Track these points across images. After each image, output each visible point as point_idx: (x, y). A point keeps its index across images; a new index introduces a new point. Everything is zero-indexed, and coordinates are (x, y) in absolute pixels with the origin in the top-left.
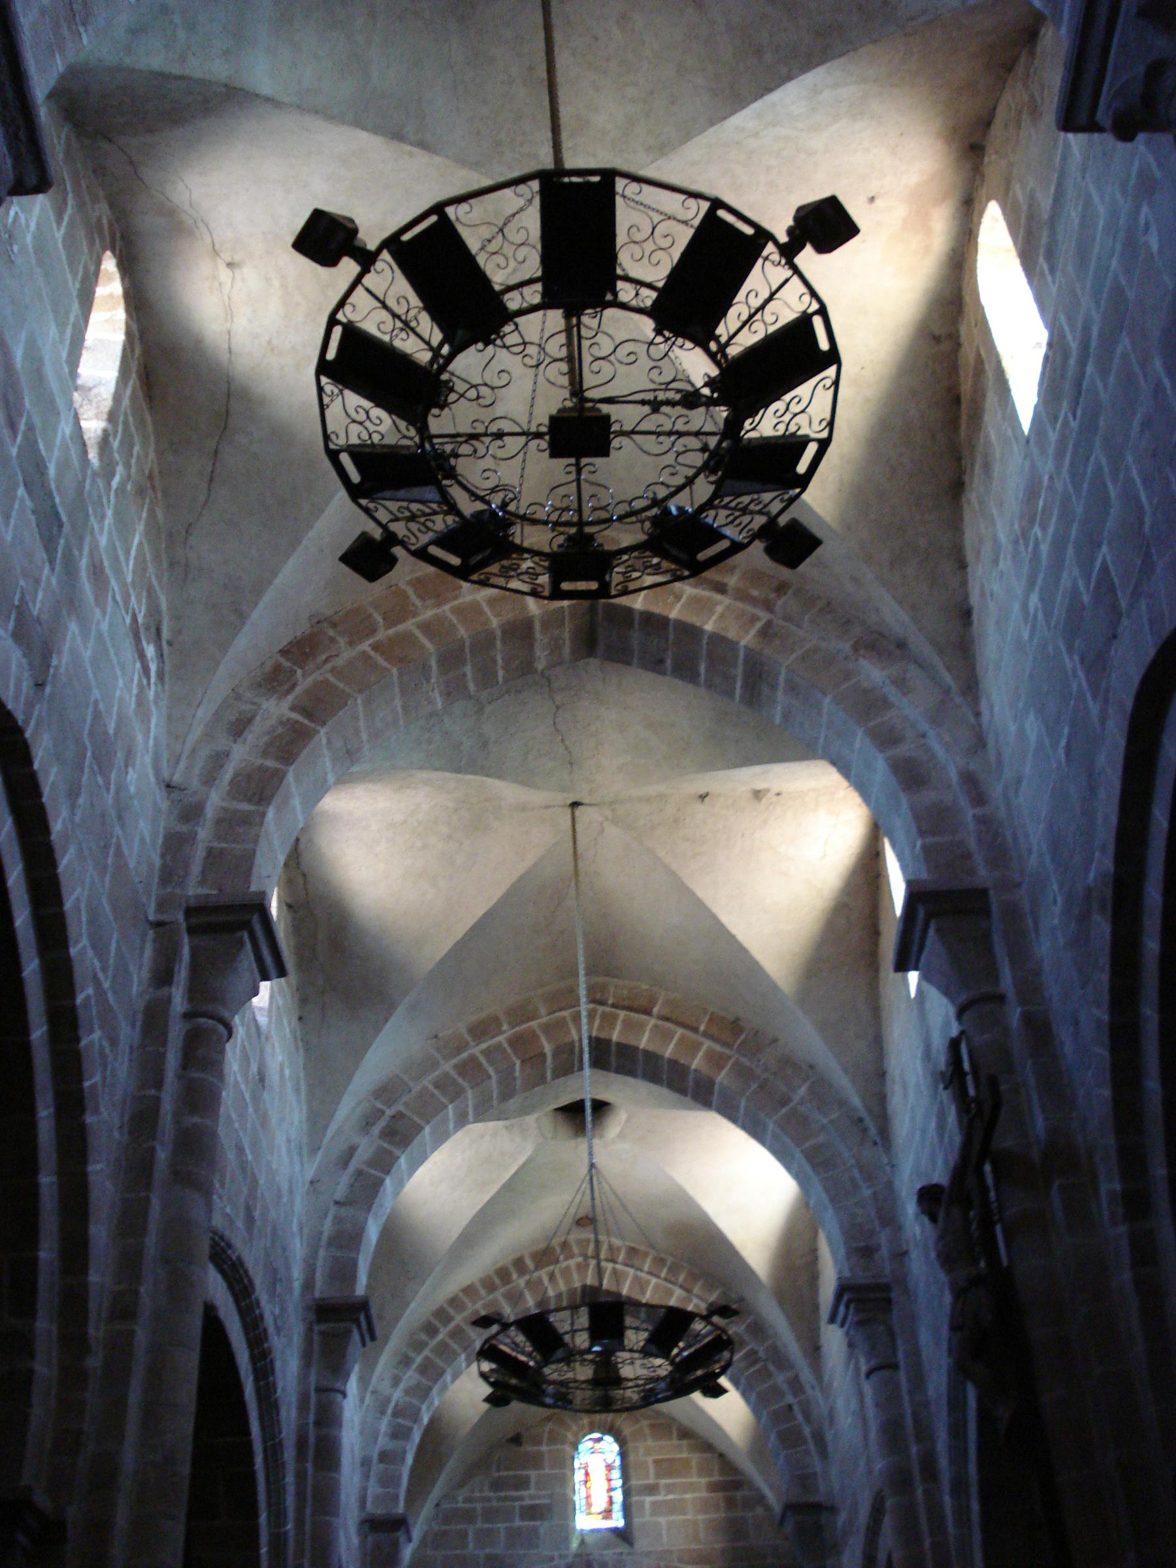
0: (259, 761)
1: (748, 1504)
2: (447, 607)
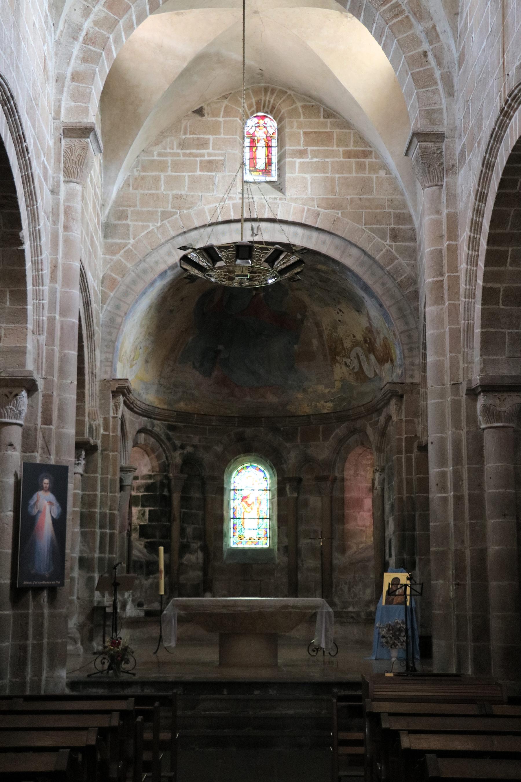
1: (373, 169)
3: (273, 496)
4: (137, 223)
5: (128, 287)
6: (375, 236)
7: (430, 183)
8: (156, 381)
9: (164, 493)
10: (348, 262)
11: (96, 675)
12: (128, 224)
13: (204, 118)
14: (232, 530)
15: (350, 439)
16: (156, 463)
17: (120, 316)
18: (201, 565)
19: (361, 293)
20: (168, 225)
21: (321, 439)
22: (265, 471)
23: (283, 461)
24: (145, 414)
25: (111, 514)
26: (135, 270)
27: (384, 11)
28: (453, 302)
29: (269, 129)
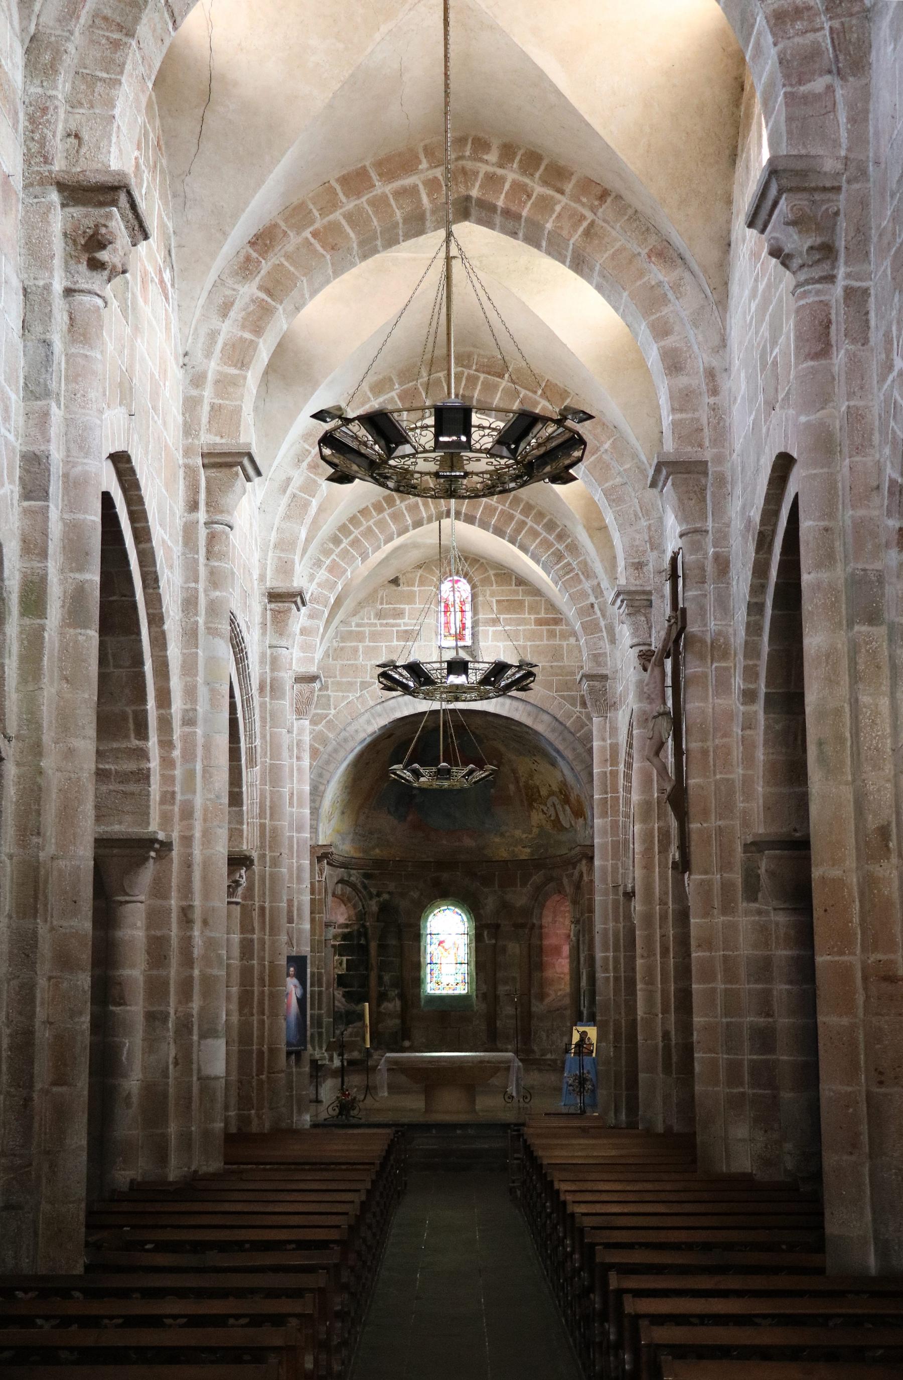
0: (240, 333)
1: (564, 636)
2: (364, 199)
5: (330, 755)
8: (352, 830)
10: (540, 728)
13: (399, 588)
14: (429, 976)
16: (352, 912)
27: (558, 569)
29: (463, 593)
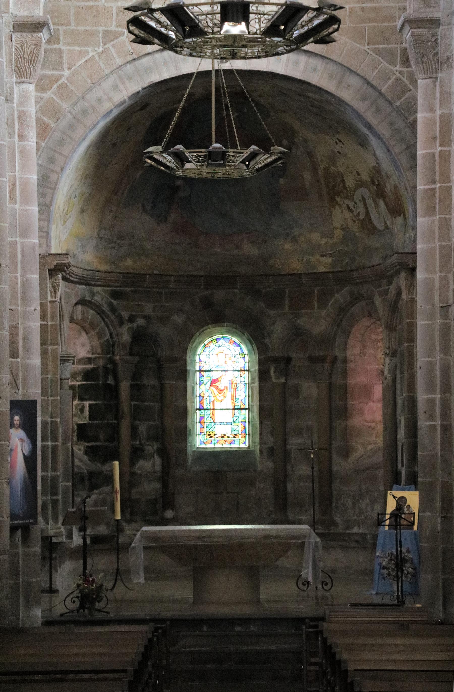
3: (253, 379)
4: (72, 48)
5: (64, 133)
6: (382, 60)
7: (424, 75)
9: (109, 382)
11: (68, 614)
12: (61, 50)
15: (353, 308)
16: (96, 343)
17: (56, 172)
18: (159, 474)
19: (365, 130)
20: (113, 50)
21: (316, 306)
22: (241, 345)
23: (266, 335)
24: (82, 281)
25: (52, 422)
26: (72, 110)
28: (443, 216)
